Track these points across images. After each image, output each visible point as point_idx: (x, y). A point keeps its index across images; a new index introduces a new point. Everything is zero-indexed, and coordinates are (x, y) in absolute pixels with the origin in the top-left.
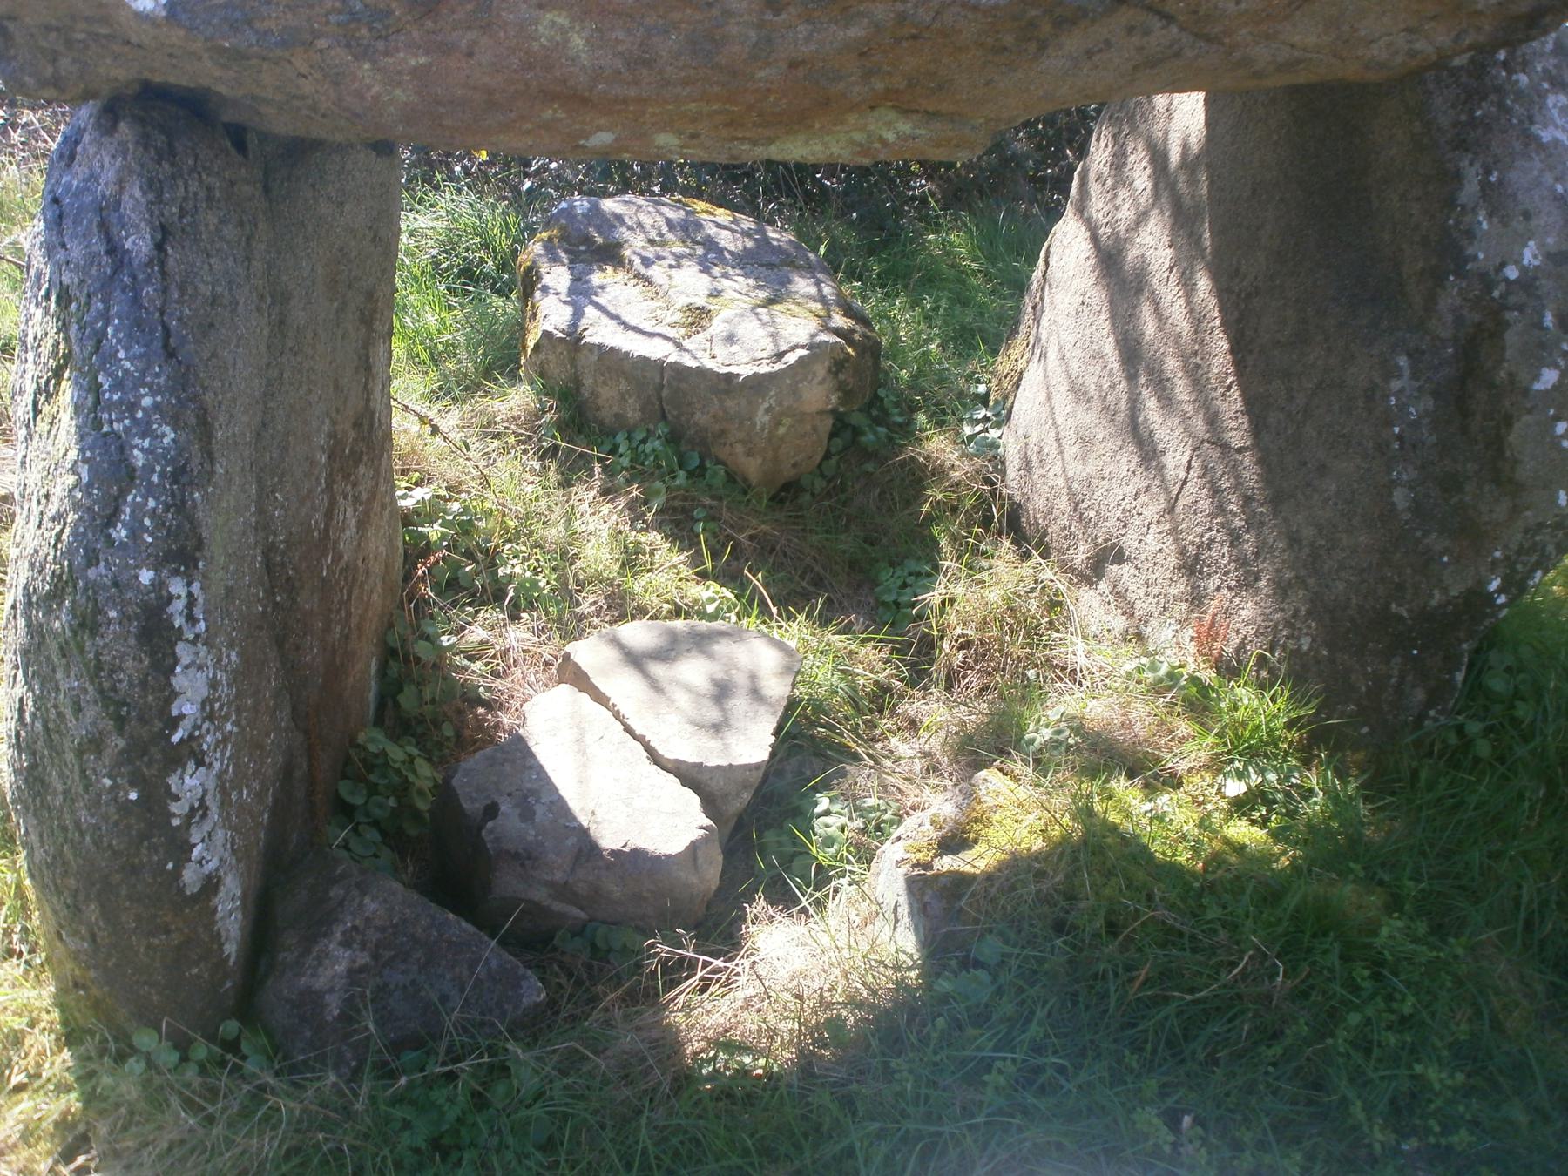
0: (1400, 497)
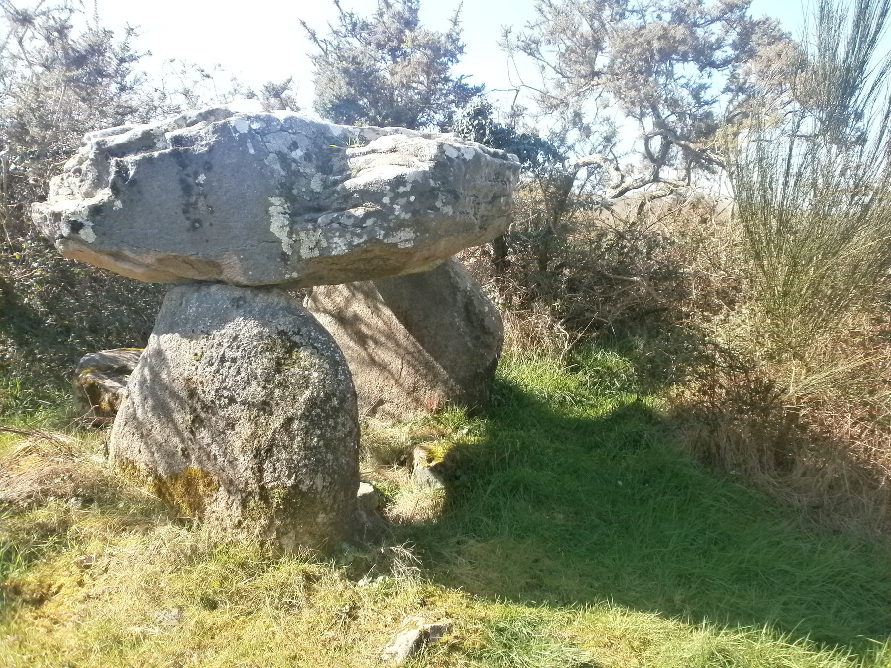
0: (470, 344)
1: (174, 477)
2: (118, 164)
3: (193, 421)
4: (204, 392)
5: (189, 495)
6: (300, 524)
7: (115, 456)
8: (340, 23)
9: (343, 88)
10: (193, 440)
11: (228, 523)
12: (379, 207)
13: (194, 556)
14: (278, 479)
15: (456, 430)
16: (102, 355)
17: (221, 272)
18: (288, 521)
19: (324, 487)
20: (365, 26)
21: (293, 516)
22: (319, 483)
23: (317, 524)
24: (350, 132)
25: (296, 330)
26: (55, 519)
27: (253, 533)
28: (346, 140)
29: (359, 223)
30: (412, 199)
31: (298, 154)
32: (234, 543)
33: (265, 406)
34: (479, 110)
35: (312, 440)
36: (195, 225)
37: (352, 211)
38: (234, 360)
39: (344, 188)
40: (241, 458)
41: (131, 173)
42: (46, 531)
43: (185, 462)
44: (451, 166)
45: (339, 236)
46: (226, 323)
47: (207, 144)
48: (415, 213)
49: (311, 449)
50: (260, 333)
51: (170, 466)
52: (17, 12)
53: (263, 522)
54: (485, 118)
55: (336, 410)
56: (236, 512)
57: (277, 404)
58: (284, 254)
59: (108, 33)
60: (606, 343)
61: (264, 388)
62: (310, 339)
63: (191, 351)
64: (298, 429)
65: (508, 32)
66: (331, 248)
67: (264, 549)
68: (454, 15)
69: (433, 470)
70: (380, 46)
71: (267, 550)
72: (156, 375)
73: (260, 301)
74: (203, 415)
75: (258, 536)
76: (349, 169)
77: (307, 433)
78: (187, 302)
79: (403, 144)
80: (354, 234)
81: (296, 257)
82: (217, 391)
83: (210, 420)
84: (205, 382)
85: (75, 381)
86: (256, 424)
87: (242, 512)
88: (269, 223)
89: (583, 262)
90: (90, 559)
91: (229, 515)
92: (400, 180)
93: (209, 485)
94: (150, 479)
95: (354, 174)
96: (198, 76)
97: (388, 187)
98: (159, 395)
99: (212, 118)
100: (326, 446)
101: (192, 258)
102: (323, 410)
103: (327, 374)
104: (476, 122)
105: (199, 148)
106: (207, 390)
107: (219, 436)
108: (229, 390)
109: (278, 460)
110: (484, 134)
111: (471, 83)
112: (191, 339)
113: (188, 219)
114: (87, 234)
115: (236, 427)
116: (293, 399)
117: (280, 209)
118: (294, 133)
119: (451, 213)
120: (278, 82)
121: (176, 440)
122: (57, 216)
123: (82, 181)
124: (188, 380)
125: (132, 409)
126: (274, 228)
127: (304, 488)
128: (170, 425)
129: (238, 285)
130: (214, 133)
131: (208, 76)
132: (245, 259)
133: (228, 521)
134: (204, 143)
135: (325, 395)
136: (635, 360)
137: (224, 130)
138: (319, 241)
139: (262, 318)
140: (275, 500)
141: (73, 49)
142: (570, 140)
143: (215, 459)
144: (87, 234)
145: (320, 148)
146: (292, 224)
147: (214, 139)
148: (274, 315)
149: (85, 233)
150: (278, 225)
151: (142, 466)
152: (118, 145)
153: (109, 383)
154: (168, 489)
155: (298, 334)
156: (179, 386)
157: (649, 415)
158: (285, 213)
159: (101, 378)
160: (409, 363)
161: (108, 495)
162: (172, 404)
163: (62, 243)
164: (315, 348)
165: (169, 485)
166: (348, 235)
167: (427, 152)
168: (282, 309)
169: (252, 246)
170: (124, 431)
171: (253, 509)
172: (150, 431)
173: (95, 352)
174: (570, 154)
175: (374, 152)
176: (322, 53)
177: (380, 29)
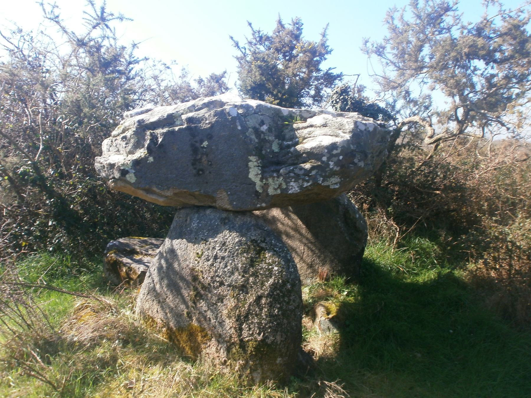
0: (347, 238)
1: (181, 329)
2: (151, 134)
3: (196, 296)
4: (203, 278)
5: (191, 342)
6: (265, 364)
7: (140, 313)
8: (252, 37)
9: (257, 76)
10: (195, 308)
11: (217, 361)
12: (319, 163)
13: (198, 384)
14: (252, 334)
15: (340, 292)
16: (119, 242)
17: (215, 202)
18: (257, 362)
19: (281, 341)
20: (268, 38)
21: (261, 359)
22: (278, 338)
23: (276, 365)
24: (294, 113)
25: (263, 239)
26: (108, 355)
27: (234, 369)
28: (291, 118)
29: (307, 172)
30: (341, 157)
31: (264, 128)
32: (221, 375)
33: (244, 288)
34: (343, 89)
35: (274, 310)
36: (200, 172)
37: (302, 165)
38: (223, 258)
39: (296, 150)
40: (227, 321)
41: (160, 140)
42: (103, 363)
43: (189, 321)
44: (363, 136)
45: (294, 182)
46: (218, 234)
47: (209, 123)
48: (342, 166)
49: (274, 317)
50: (240, 241)
51: (178, 322)
52: (78, 40)
53: (241, 362)
54: (348, 95)
55: (289, 291)
56: (223, 355)
57: (252, 287)
58: (257, 192)
59: (123, 48)
60: (420, 232)
61: (243, 276)
62: (271, 245)
63: (195, 251)
64: (265, 304)
65: (367, 42)
66: (288, 189)
67: (242, 380)
68: (323, 31)
69: (332, 320)
70: (278, 50)
71: (244, 381)
72: (170, 265)
73: (239, 221)
74: (202, 292)
75: (237, 371)
76: (297, 137)
77: (271, 306)
78: (191, 220)
79: (331, 122)
80: (304, 180)
81: (265, 194)
82: (212, 278)
83: (207, 295)
84: (204, 271)
85: (105, 258)
86: (238, 299)
87: (227, 355)
88: (248, 173)
89: (404, 182)
90: (131, 383)
91: (218, 357)
92: (334, 146)
93: (205, 336)
94: (164, 329)
95: (300, 141)
96: (162, 68)
97: (326, 151)
98: (171, 275)
99: (212, 106)
100: (283, 314)
101: (197, 193)
102: (281, 292)
103: (283, 268)
104: (342, 97)
105: (205, 125)
106: (206, 276)
107: (212, 306)
108: (220, 277)
109: (252, 323)
110: (347, 104)
111: (335, 72)
112: (194, 243)
113: (195, 169)
114: (131, 177)
115: (224, 300)
116: (262, 284)
117: (256, 164)
118: (262, 115)
119: (363, 166)
120: (218, 73)
121: (183, 307)
122: (112, 166)
123: (126, 144)
124: (193, 270)
125: (152, 285)
126: (251, 176)
127: (269, 341)
128: (179, 297)
129: (227, 210)
130: (214, 116)
131: (168, 68)
132: (231, 194)
133: (218, 360)
134: (207, 122)
135: (283, 282)
136: (439, 244)
137: (222, 114)
138: (281, 184)
139: (241, 232)
140: (250, 348)
141: (104, 58)
142: (398, 106)
143: (210, 320)
144: (131, 177)
145: (277, 123)
146: (263, 173)
147: (214, 120)
148: (248, 229)
149: (130, 177)
150: (254, 173)
151: (159, 321)
152: (151, 122)
153: (125, 260)
154: (176, 337)
155: (264, 242)
156: (186, 273)
157: (457, 281)
158: (259, 166)
159: (121, 257)
160: (309, 248)
161: (137, 339)
162: (181, 284)
163: (113, 182)
164: (275, 251)
165: (177, 334)
166: (300, 181)
167: (347, 127)
168: (253, 225)
169: (236, 186)
170: (147, 298)
171: (235, 354)
172: (165, 299)
173: (115, 240)
174: (398, 116)
175: (311, 126)
176: (242, 55)
177: (277, 40)
